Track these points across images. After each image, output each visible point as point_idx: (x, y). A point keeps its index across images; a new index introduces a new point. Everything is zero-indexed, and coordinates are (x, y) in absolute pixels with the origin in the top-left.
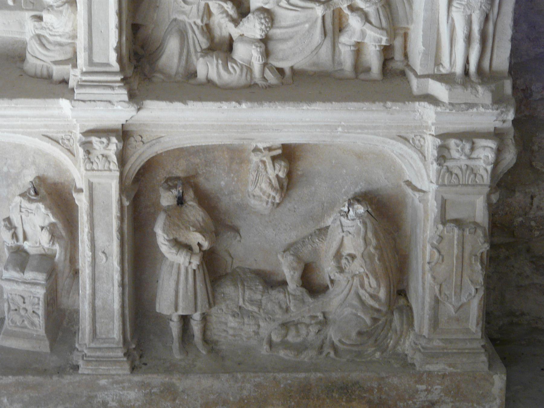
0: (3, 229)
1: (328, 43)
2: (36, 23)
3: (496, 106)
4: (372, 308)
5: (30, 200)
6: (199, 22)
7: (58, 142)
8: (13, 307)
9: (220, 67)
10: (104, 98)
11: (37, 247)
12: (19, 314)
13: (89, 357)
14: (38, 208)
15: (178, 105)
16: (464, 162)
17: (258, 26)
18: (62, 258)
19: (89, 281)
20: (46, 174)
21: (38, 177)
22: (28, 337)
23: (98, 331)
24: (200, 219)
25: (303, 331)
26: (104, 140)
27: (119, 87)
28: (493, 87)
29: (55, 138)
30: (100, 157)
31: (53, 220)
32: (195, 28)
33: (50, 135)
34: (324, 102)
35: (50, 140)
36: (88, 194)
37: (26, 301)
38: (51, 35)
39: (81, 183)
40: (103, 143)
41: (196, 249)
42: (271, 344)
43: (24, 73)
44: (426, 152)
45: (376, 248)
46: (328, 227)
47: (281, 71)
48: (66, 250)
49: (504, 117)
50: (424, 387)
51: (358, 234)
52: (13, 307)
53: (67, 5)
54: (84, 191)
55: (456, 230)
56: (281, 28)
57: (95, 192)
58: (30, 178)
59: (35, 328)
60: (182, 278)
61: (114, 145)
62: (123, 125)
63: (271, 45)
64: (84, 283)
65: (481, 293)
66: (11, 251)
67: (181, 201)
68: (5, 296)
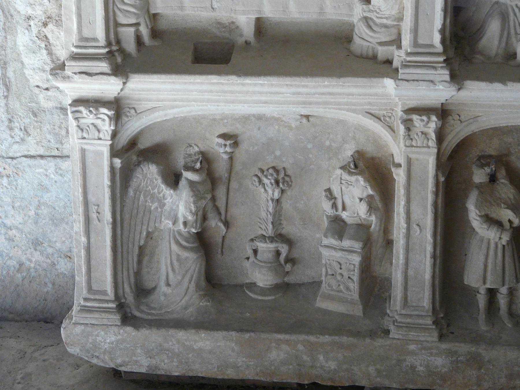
0: (324, 198)
2: (364, 6)
5: (350, 173)
10: (427, 78)
11: (354, 217)
13: (399, 322)
14: (357, 180)
15: (498, 86)
18: (377, 228)
19: (403, 251)
20: (364, 148)
21: (358, 152)
22: (342, 301)
23: (409, 299)
24: (512, 197)
26: (425, 118)
27: (442, 67)
29: (377, 115)
30: (420, 134)
31: (371, 192)
33: (372, 112)
35: (373, 117)
36: (406, 169)
37: (343, 267)
38: (377, 17)
39: (399, 159)
40: (424, 121)
41: (507, 225)
43: (350, 53)
44: (76, 94)
48: (381, 221)
54: (403, 165)
57: (412, 168)
58: (349, 153)
59: (350, 293)
60: (492, 253)
61: (434, 123)
62: (442, 104)
64: (398, 253)
66: (330, 220)
67: (493, 179)
68: (324, 262)
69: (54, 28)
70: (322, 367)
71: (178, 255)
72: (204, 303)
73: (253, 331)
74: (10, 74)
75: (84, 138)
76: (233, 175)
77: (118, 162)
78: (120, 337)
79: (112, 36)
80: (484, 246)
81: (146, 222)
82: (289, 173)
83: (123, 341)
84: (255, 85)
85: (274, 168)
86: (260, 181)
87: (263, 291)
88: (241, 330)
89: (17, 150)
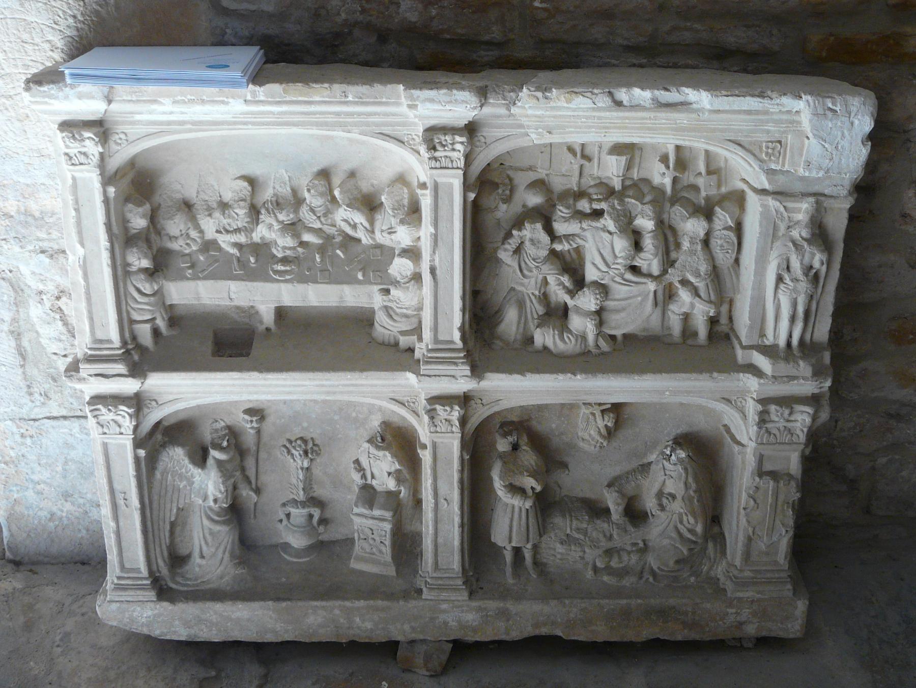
1: (658, 311)
3: (815, 378)
4: (689, 540)
5: (378, 448)
6: (537, 293)
7: (404, 405)
8: (362, 536)
9: (557, 337)
10: (448, 373)
12: (368, 542)
14: (385, 455)
15: (517, 377)
16: (782, 424)
17: (593, 301)
24: (534, 464)
25: (625, 557)
26: (448, 408)
27: (462, 363)
28: (813, 361)
30: (444, 421)
31: (398, 467)
32: (533, 298)
33: (397, 398)
34: (654, 373)
41: (530, 492)
42: (595, 569)
45: (695, 492)
46: (650, 464)
47: (613, 338)
49: (822, 385)
50: (734, 611)
51: (680, 479)
52: (362, 536)
53: (413, 282)
55: (771, 483)
56: (615, 300)
61: (456, 413)
63: (605, 315)
64: (427, 522)
65: (791, 533)
67: (515, 447)
69: (68, 301)
70: (359, 628)
71: (210, 529)
72: (239, 571)
73: (289, 600)
74: (25, 343)
75: (105, 433)
76: (261, 446)
77: (142, 453)
78: (156, 612)
79: (127, 335)
80: (509, 510)
81: (175, 500)
82: (317, 442)
83: (160, 615)
84: (278, 379)
85: (301, 438)
86: (289, 452)
87: (299, 553)
88: (278, 599)
89: (38, 412)
